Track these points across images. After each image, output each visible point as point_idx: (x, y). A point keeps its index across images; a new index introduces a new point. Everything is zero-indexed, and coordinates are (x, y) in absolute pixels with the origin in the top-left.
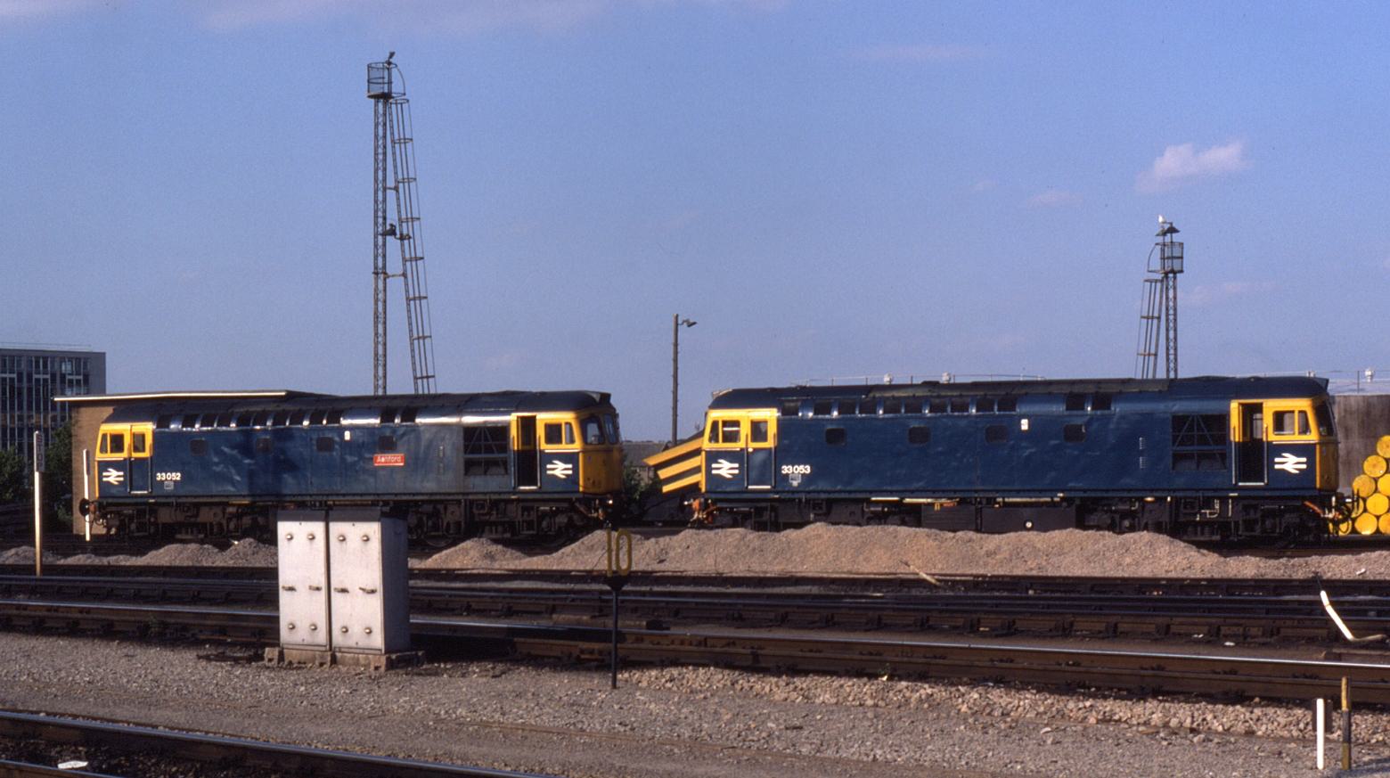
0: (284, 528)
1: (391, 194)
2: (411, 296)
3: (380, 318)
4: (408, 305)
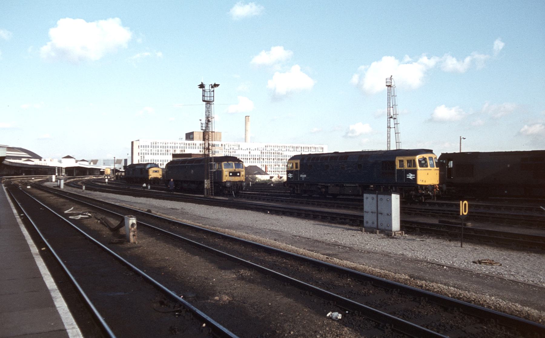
0: (365, 195)
1: (391, 108)
2: (394, 114)
3: (389, 137)
4: (396, 135)
